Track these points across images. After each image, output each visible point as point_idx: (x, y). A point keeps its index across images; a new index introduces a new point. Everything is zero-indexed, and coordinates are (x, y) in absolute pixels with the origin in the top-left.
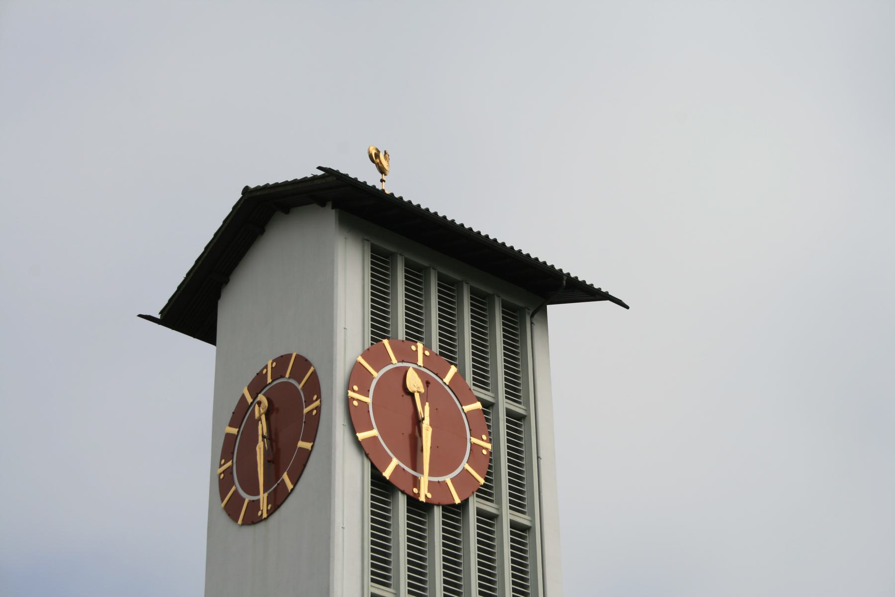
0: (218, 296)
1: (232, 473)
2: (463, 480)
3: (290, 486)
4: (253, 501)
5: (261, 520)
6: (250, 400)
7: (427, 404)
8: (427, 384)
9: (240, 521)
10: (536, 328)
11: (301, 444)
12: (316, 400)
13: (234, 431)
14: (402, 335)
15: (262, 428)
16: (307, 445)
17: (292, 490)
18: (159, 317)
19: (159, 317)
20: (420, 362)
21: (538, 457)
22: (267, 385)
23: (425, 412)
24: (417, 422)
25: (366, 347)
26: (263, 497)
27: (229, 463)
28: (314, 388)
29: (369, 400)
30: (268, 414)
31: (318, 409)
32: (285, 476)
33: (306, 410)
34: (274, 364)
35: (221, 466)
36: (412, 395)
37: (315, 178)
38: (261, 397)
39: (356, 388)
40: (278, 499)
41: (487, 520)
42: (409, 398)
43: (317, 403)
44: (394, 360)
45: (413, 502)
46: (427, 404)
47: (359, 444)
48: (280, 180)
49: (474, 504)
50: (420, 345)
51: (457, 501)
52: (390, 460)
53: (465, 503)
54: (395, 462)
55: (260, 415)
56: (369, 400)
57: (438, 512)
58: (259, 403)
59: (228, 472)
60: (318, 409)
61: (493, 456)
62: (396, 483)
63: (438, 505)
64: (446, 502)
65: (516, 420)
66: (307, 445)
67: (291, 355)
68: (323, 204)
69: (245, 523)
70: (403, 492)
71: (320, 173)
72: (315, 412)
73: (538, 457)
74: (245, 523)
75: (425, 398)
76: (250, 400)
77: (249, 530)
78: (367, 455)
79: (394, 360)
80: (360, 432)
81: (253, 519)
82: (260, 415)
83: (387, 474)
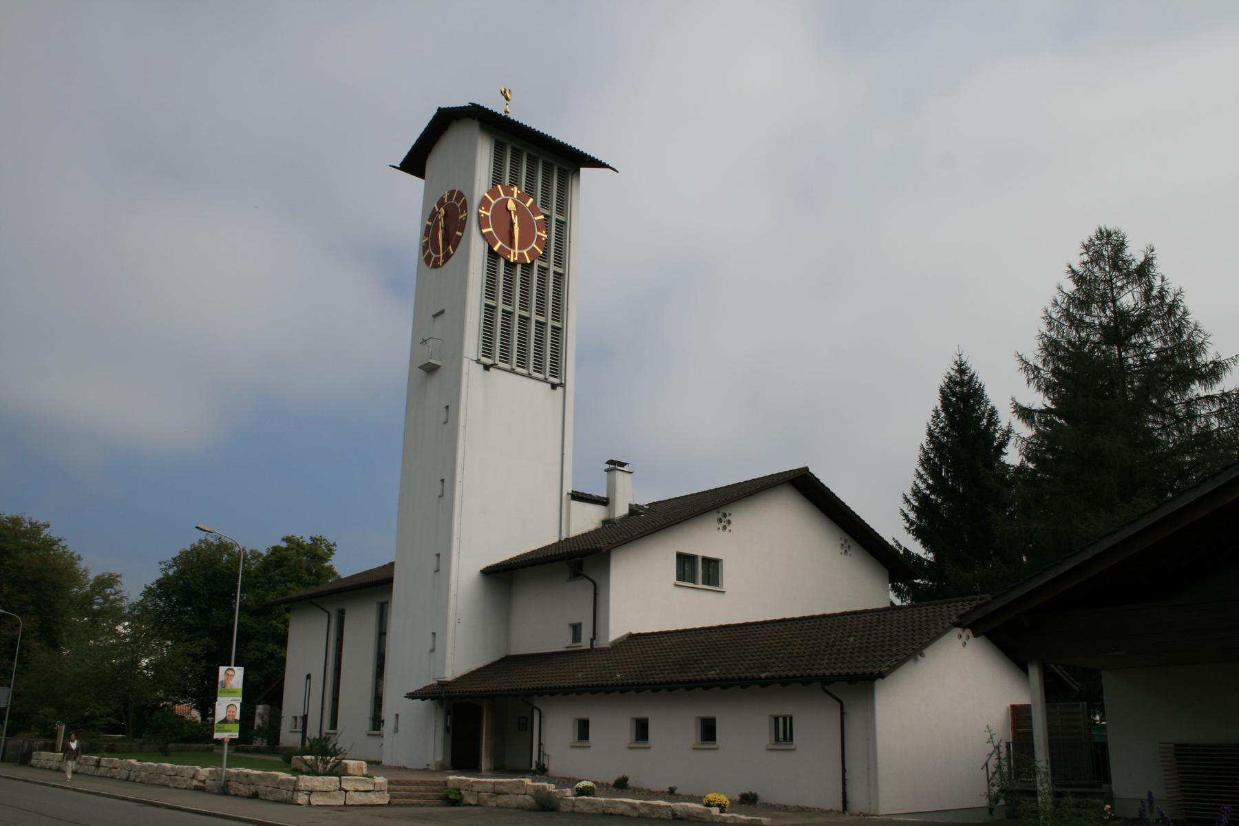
5: (439, 266)
13: (430, 223)
14: (507, 183)
18: (399, 166)
23: (515, 220)
27: (427, 239)
29: (489, 214)
30: (444, 217)
31: (466, 217)
36: (510, 212)
40: (447, 257)
43: (465, 214)
45: (507, 262)
50: (516, 188)
52: (498, 242)
56: (489, 214)
57: (519, 267)
60: (466, 217)
62: (500, 253)
65: (561, 224)
68: (473, 118)
70: (503, 257)
81: (436, 266)
83: (496, 249)
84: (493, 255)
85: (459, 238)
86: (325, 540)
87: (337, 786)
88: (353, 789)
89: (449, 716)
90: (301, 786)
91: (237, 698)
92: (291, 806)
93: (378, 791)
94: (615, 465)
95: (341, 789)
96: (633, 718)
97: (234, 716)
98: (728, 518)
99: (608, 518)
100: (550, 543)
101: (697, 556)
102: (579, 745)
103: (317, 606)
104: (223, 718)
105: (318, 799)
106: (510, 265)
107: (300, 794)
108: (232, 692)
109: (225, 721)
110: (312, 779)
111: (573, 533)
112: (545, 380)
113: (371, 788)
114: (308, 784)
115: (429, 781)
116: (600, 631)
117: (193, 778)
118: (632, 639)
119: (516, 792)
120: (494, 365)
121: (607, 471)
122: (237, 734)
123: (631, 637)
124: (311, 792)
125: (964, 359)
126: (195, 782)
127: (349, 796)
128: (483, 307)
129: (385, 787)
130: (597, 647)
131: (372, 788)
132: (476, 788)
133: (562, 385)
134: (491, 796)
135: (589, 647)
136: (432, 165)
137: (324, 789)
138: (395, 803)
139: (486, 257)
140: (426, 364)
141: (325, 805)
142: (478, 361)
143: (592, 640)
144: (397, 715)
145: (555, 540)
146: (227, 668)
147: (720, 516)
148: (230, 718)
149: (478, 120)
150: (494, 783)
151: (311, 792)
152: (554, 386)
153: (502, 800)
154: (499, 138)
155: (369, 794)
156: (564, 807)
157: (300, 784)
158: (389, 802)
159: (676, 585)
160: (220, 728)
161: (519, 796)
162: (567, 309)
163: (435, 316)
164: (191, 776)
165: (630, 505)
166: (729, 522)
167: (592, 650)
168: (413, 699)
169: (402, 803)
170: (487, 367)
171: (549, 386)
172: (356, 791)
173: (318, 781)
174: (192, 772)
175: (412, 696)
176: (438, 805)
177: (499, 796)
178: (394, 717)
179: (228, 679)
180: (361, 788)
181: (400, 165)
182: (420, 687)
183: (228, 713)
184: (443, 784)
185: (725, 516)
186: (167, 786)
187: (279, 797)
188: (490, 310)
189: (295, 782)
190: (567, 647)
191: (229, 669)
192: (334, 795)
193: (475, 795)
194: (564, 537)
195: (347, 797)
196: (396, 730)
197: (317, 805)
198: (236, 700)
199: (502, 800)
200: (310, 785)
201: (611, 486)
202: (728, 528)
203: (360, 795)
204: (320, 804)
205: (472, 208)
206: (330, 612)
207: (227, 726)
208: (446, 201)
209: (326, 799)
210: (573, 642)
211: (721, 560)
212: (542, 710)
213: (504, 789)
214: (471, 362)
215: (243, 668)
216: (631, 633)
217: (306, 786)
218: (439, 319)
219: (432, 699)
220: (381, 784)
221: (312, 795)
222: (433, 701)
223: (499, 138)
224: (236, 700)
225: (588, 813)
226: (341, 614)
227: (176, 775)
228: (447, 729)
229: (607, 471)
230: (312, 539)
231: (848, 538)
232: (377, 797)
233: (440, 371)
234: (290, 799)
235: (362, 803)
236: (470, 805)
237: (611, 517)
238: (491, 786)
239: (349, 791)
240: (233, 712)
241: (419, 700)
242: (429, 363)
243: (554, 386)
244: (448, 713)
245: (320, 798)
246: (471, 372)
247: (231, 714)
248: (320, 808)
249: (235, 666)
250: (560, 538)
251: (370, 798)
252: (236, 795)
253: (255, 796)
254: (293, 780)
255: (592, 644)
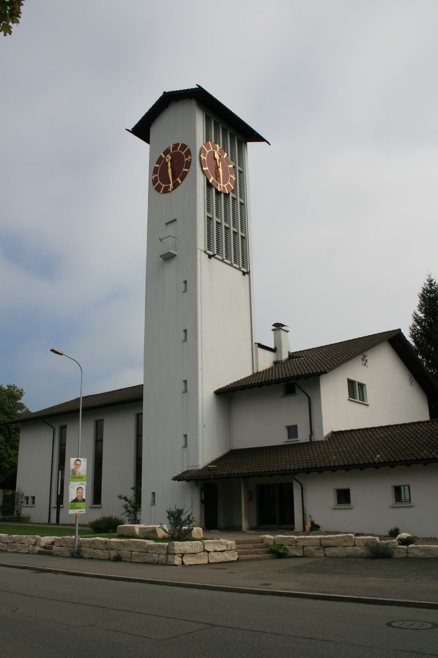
0: (150, 126)
1: (157, 178)
2: (228, 186)
3: (180, 182)
4: (166, 186)
5: (169, 192)
6: (164, 156)
7: (220, 162)
8: (220, 156)
9: (161, 192)
10: (245, 148)
11: (184, 170)
12: (190, 157)
13: (158, 166)
14: (213, 141)
15: (169, 165)
16: (187, 170)
17: (181, 183)
18: (131, 130)
19: (131, 130)
20: (218, 151)
21: (246, 184)
22: (170, 152)
23: (220, 164)
24: (217, 168)
25: (205, 143)
26: (171, 185)
27: (156, 175)
28: (189, 153)
29: (206, 159)
30: (171, 161)
31: (191, 159)
32: (178, 179)
33: (186, 160)
34: (173, 146)
35: (153, 176)
36: (216, 160)
37: (196, 88)
38: (168, 156)
39: (202, 154)
40: (176, 185)
41: (234, 199)
42: (215, 160)
43: (190, 158)
44: (212, 149)
45: (216, 190)
46: (220, 162)
47: (203, 171)
48: (178, 90)
49: (231, 195)
50: (218, 145)
51: (227, 193)
52: (211, 177)
53: (229, 193)
54: (212, 178)
55: (168, 161)
56: (206, 159)
57: (222, 195)
58: (168, 158)
59: (156, 178)
60: (191, 159)
61: (236, 180)
62: (213, 184)
63: (223, 193)
64: (225, 192)
65: (240, 172)
66: (187, 170)
67: (179, 144)
68: (191, 98)
69: (163, 192)
70: (214, 187)
71: (197, 87)
72: (189, 160)
73: (246, 184)
74: (163, 192)
75: (219, 161)
76: (164, 156)
77: (165, 195)
78: (205, 175)
79: (212, 149)
80: (204, 167)
81: (166, 191)
82: (168, 161)
83: (210, 181)
84: (209, 185)
85: (186, 173)
86: (16, 387)
87: (202, 549)
88: (213, 551)
89: (203, 493)
90: (176, 550)
91: (84, 483)
92: (166, 567)
93: (230, 551)
94: (278, 326)
95: (205, 551)
96: (392, 486)
97: (82, 496)
98: (366, 358)
99: (276, 360)
100: (246, 376)
101: (355, 381)
102: (397, 505)
103: (48, 424)
104: (74, 498)
105: (189, 560)
106: (218, 193)
107: (176, 557)
108: (80, 478)
109: (76, 500)
110: (183, 544)
111: (261, 369)
112: (239, 269)
113: (225, 548)
114: (181, 548)
115: (252, 540)
116: (315, 430)
117: (35, 544)
118: (334, 434)
119: (345, 545)
120: (214, 256)
121: (273, 330)
122: (84, 510)
123: (334, 433)
124: (183, 554)
125: (432, 277)
126: (38, 548)
127: (211, 556)
128: (206, 218)
129: (234, 547)
130: (315, 440)
131: (226, 549)
132: (301, 544)
133: (248, 273)
134: (318, 549)
135: (309, 441)
136: (154, 132)
137: (193, 552)
138: (242, 559)
139: (206, 187)
140: (169, 252)
141: (195, 565)
142: (205, 252)
143: (311, 436)
144: (154, 494)
145: (250, 373)
146: (76, 459)
147: (362, 356)
148: (79, 498)
149: (195, 100)
150: (320, 538)
151: (183, 554)
152: (244, 273)
153: (329, 551)
154: (208, 114)
155: (224, 553)
156: (397, 554)
157: (175, 549)
158: (238, 559)
159: (349, 400)
160: (73, 505)
161: (348, 548)
162: (248, 226)
163: (167, 224)
164: (33, 543)
165: (289, 352)
166: (367, 361)
167: (311, 443)
168: (178, 481)
169: (246, 558)
170: (210, 257)
171: (241, 273)
172: (215, 551)
173: (188, 545)
174: (33, 541)
175: (175, 479)
176: (269, 558)
177: (327, 549)
178: (151, 494)
179: (77, 467)
180: (218, 549)
181: (132, 129)
182: (180, 472)
183: (78, 494)
184: (261, 541)
185: (365, 356)
186: (6, 551)
187: (150, 559)
188: (209, 219)
189: (168, 546)
190: (285, 442)
191: (77, 460)
192: (200, 556)
193: (301, 548)
194: (255, 371)
195: (210, 557)
196: (153, 503)
197: (190, 565)
198: (83, 484)
199: (329, 551)
200: (183, 549)
201: (278, 340)
202: (367, 364)
203: (218, 555)
204: (192, 563)
205: (195, 154)
206: (55, 428)
207: (78, 504)
208: (171, 151)
209: (194, 559)
210: (289, 438)
211: (365, 385)
212: (303, 484)
213: (332, 543)
214: (201, 251)
215: (71, 458)
216: (333, 431)
217: (180, 550)
218: (171, 226)
219: (188, 481)
220: (231, 545)
221: (184, 557)
222: (189, 482)
223: (208, 114)
224: (83, 484)
225: (422, 558)
226: (63, 428)
227: (14, 543)
228: (202, 501)
229: (273, 330)
230: (9, 386)
231: (412, 375)
232: (229, 555)
233: (175, 259)
234: (164, 561)
235: (220, 561)
236: (296, 556)
237: (279, 359)
238: (317, 541)
239: (210, 552)
240: (81, 493)
241: (185, 481)
242: (170, 252)
243: (244, 273)
244: (202, 490)
245: (190, 559)
246: (202, 258)
247: (80, 495)
248: (192, 567)
249: (80, 458)
250: (253, 372)
251: (225, 556)
252: (92, 558)
253: (118, 559)
254: (165, 545)
255: (311, 439)
